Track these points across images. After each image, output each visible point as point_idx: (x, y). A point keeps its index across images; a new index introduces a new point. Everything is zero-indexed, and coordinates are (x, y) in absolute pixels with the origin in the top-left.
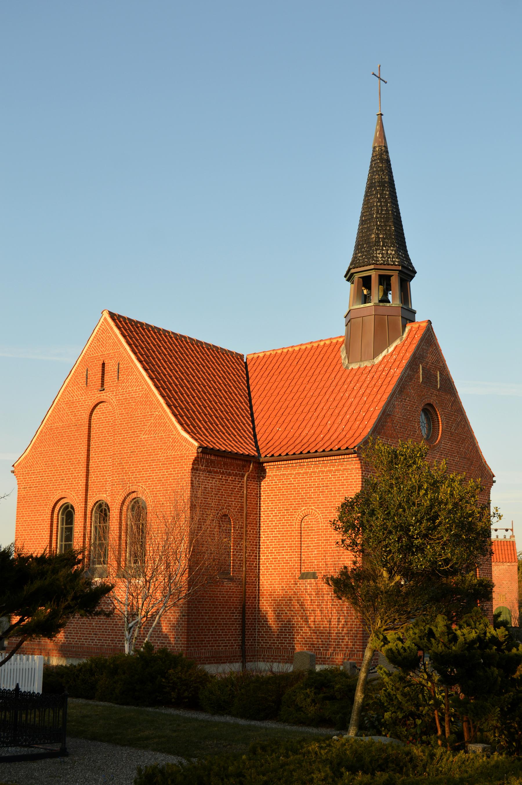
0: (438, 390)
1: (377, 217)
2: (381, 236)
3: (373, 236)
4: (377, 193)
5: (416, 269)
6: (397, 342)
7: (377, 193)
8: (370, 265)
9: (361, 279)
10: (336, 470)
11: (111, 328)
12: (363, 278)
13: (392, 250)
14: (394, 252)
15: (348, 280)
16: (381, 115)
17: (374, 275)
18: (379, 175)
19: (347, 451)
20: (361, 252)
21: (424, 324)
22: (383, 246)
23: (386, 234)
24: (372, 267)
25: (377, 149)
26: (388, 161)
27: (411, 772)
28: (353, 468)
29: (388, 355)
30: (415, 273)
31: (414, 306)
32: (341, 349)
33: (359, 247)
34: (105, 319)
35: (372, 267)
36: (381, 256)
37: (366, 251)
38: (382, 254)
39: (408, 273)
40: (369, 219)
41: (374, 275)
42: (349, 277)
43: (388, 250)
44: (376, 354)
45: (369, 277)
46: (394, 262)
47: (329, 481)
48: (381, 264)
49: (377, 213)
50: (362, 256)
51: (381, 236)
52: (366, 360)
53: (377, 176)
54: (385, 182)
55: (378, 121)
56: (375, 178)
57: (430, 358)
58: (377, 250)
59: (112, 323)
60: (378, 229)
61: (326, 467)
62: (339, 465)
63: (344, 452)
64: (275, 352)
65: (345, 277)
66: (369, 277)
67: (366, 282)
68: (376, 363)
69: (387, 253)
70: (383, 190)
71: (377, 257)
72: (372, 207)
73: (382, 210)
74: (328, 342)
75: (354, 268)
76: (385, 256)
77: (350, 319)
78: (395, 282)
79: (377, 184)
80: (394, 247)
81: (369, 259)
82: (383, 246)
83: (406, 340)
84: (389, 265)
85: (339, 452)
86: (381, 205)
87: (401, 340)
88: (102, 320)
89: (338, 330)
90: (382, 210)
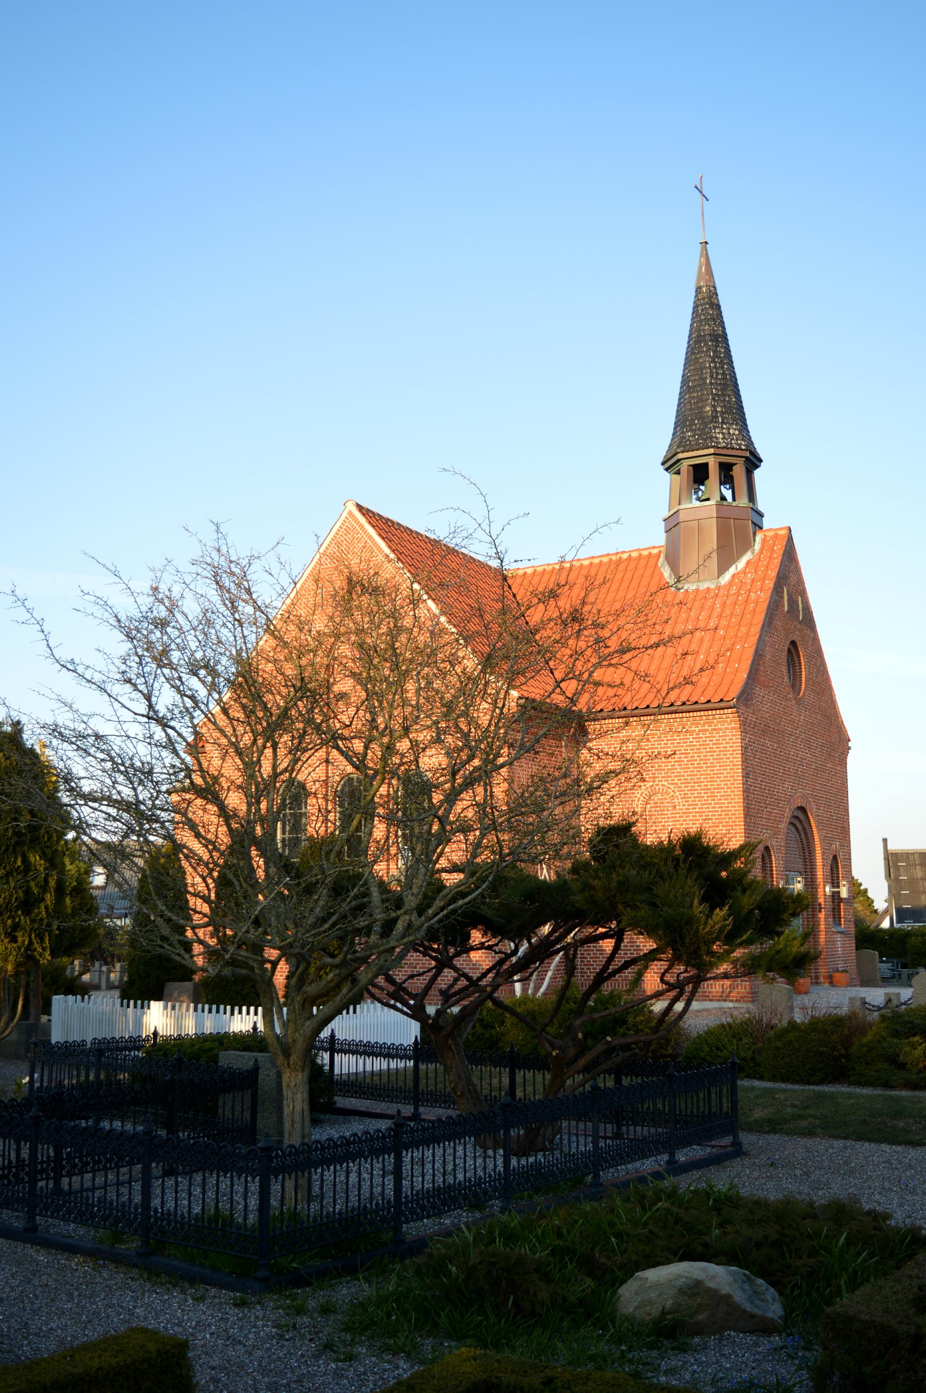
0: (800, 623)
1: (711, 383)
2: (719, 409)
3: (708, 408)
4: (708, 350)
5: (762, 457)
6: (748, 556)
7: (708, 350)
8: (708, 448)
9: (691, 468)
10: (700, 731)
11: (362, 527)
12: (695, 467)
13: (735, 429)
14: (737, 432)
15: (667, 469)
16: (706, 243)
17: (713, 463)
18: (710, 325)
19: (722, 705)
20: (691, 430)
21: (784, 532)
22: (723, 422)
23: (725, 406)
24: (712, 451)
25: (704, 289)
26: (718, 307)
27: (77, 968)
28: (727, 729)
29: (738, 574)
30: (761, 461)
31: (761, 506)
32: (659, 564)
33: (682, 422)
34: (350, 513)
35: (712, 451)
36: (721, 436)
37: (699, 429)
38: (723, 433)
39: (753, 461)
40: (700, 386)
41: (713, 463)
42: (670, 464)
43: (729, 429)
44: (722, 571)
45: (706, 465)
46: (740, 445)
47: (689, 746)
48: (723, 448)
49: (712, 377)
50: (694, 436)
51: (719, 409)
52: (706, 580)
53: (707, 327)
54: (718, 335)
55: (702, 251)
56: (704, 330)
57: (793, 579)
58: (715, 428)
59: (362, 520)
60: (713, 399)
61: (697, 725)
62: (704, 723)
63: (717, 705)
64: (551, 567)
65: (663, 464)
66: (706, 465)
67: (700, 474)
68: (723, 584)
69: (729, 433)
70: (717, 346)
71: (716, 438)
72: (702, 369)
73: (717, 374)
74: (635, 554)
75: (683, 452)
76: (727, 436)
77: (672, 524)
78: (739, 472)
79: (708, 338)
80: (736, 424)
81: (705, 440)
82: (723, 422)
83: (761, 552)
84: (733, 448)
85: (709, 706)
86: (715, 367)
87: (753, 553)
88: (345, 514)
89: (654, 537)
90: (717, 374)
